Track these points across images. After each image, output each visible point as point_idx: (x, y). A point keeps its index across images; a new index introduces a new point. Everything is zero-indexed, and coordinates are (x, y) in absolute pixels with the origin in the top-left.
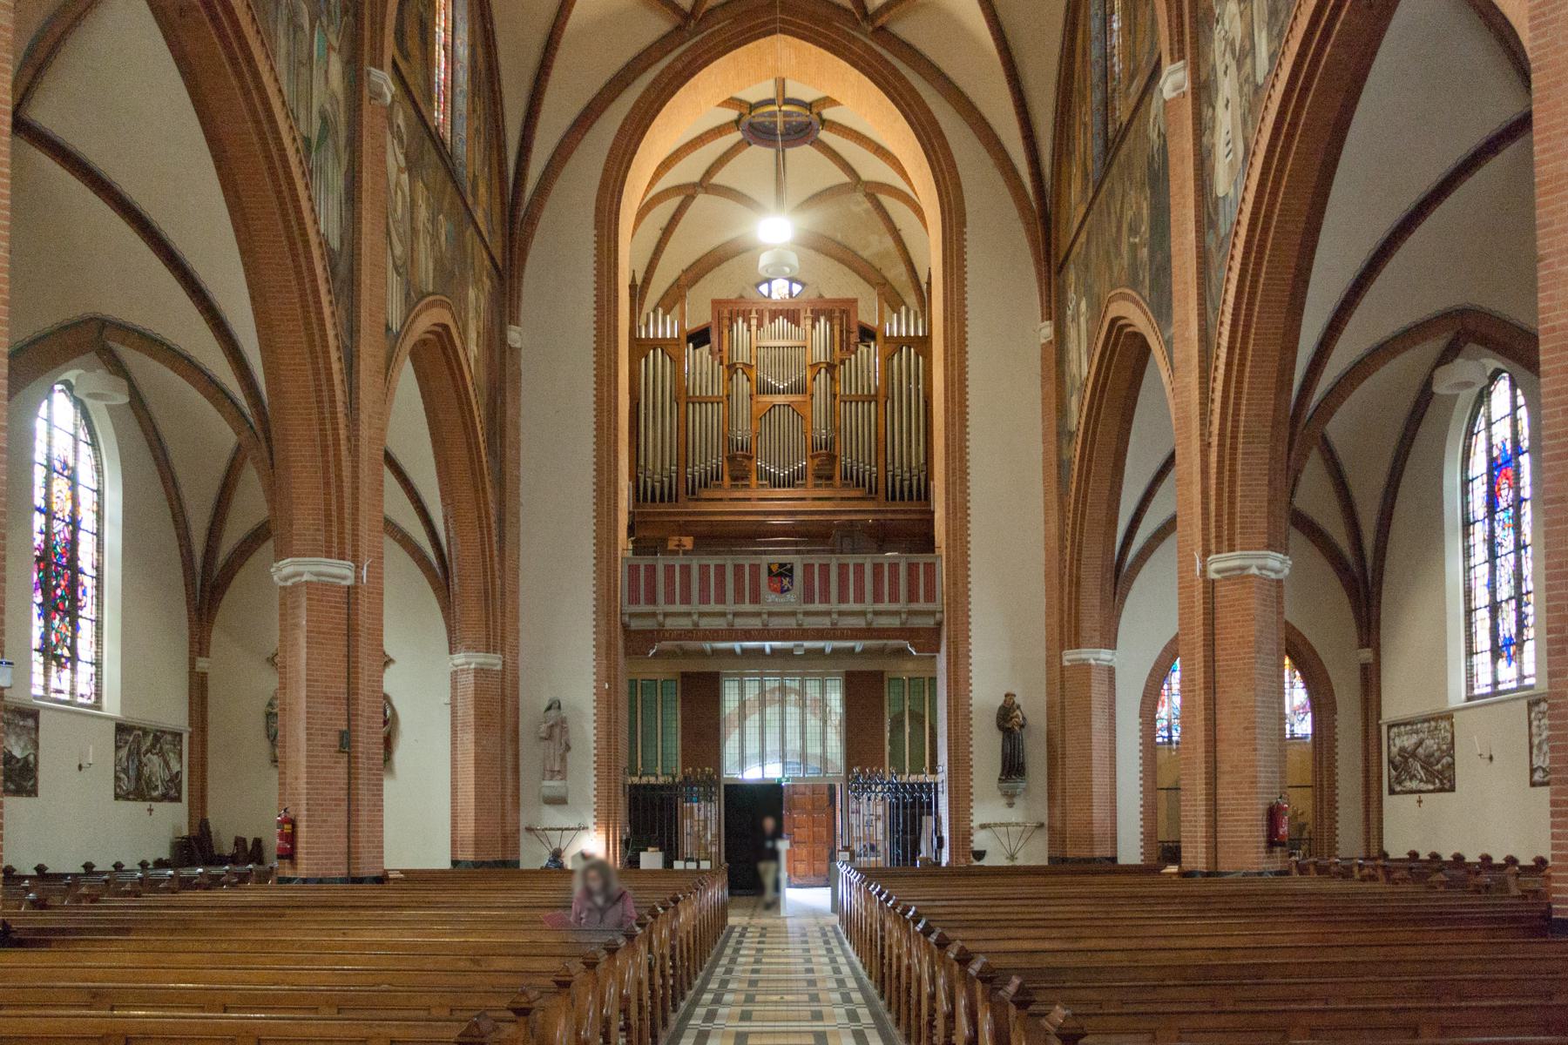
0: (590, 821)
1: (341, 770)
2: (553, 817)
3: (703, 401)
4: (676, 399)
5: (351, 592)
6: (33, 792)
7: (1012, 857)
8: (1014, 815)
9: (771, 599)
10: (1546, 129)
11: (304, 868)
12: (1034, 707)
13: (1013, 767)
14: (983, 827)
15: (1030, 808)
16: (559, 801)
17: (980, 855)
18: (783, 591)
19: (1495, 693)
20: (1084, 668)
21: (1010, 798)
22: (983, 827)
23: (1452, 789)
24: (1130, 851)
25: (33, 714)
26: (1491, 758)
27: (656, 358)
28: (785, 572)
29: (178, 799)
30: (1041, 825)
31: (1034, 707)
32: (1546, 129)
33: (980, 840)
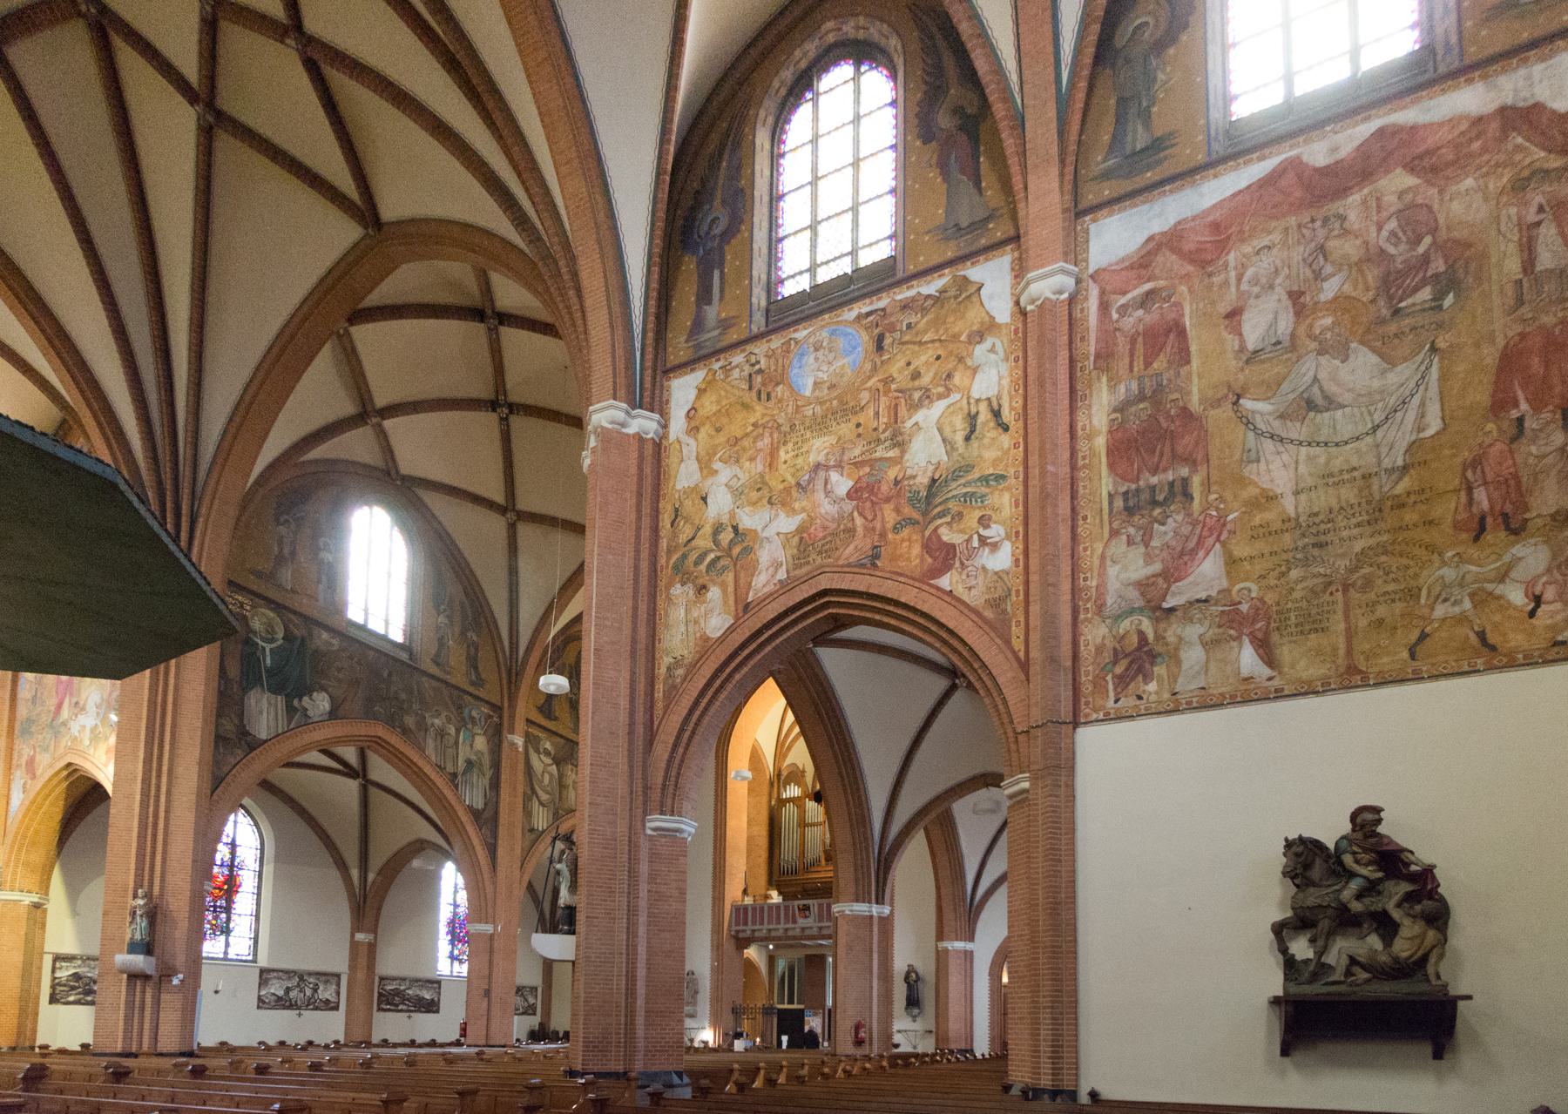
0: (707, 1025)
1: (485, 1004)
2: (689, 1023)
3: (813, 825)
4: (799, 825)
5: (492, 936)
6: (437, 1011)
7: (915, 1047)
8: (918, 1026)
9: (801, 922)
10: (387, 623)
11: (469, 1041)
12: (926, 968)
13: (913, 1002)
14: (899, 1031)
15: (927, 1021)
16: (692, 1016)
17: (897, 1046)
18: (806, 917)
19: (225, 959)
20: (946, 951)
21: (914, 1018)
22: (899, 1031)
23: (258, 1007)
24: (982, 1046)
25: (439, 982)
26: (216, 992)
27: (790, 807)
28: (806, 908)
29: (534, 1014)
30: (931, 1032)
31: (926, 968)
32: (387, 623)
33: (897, 1038)
